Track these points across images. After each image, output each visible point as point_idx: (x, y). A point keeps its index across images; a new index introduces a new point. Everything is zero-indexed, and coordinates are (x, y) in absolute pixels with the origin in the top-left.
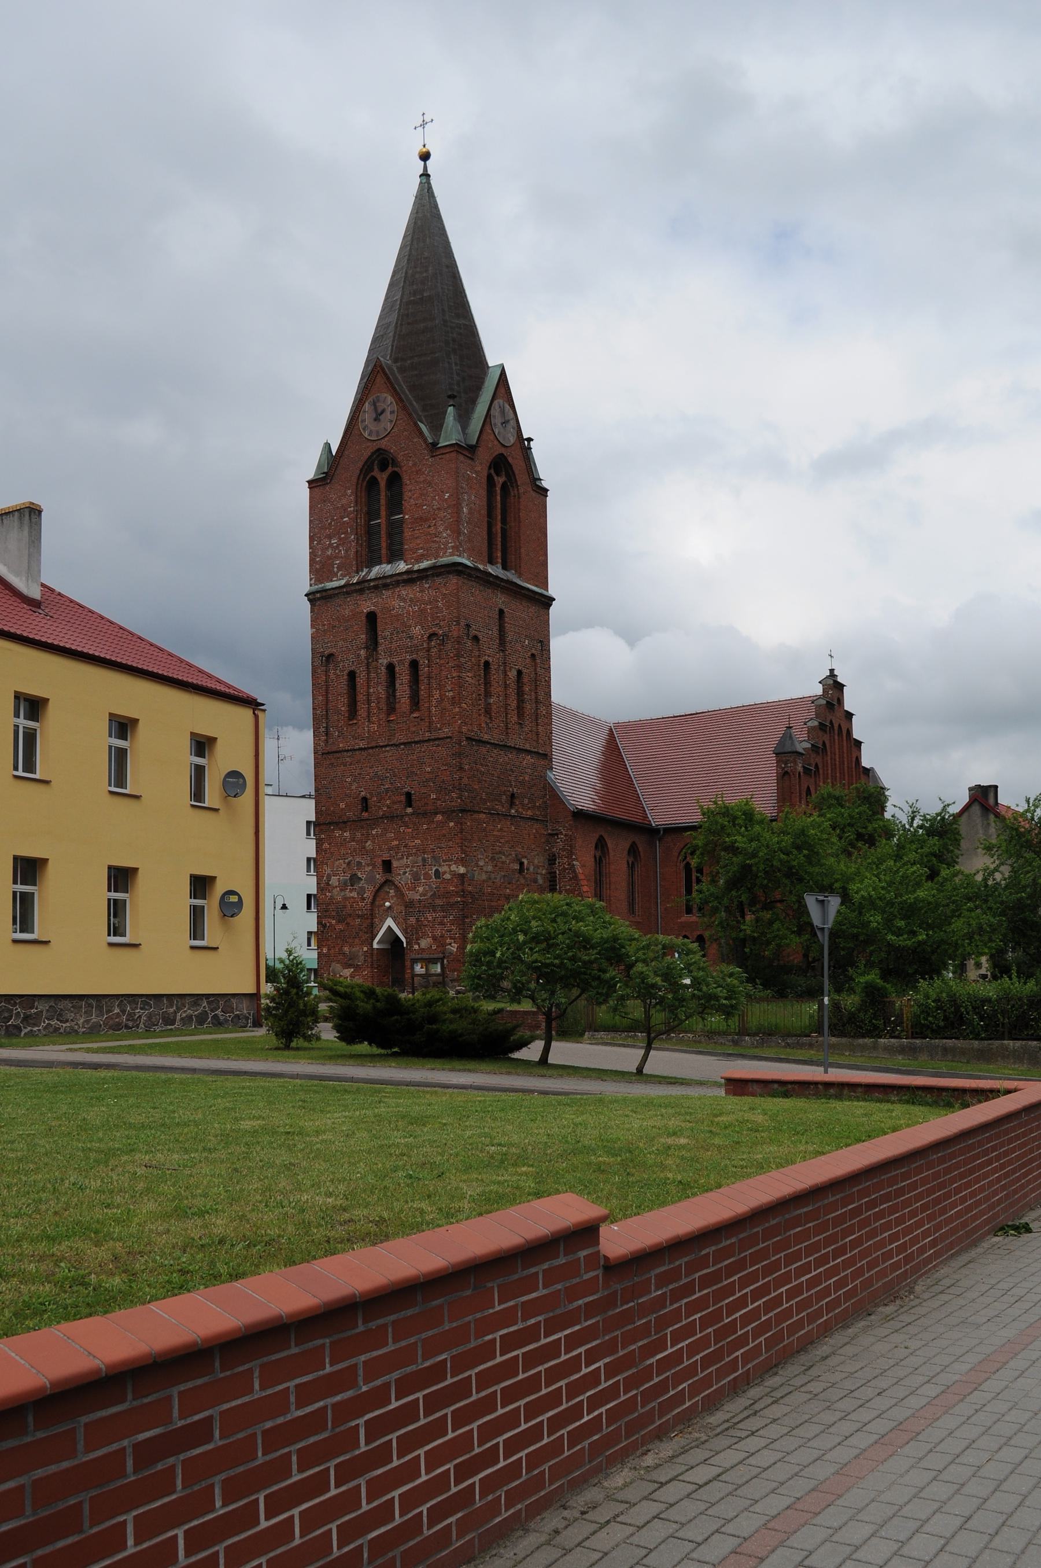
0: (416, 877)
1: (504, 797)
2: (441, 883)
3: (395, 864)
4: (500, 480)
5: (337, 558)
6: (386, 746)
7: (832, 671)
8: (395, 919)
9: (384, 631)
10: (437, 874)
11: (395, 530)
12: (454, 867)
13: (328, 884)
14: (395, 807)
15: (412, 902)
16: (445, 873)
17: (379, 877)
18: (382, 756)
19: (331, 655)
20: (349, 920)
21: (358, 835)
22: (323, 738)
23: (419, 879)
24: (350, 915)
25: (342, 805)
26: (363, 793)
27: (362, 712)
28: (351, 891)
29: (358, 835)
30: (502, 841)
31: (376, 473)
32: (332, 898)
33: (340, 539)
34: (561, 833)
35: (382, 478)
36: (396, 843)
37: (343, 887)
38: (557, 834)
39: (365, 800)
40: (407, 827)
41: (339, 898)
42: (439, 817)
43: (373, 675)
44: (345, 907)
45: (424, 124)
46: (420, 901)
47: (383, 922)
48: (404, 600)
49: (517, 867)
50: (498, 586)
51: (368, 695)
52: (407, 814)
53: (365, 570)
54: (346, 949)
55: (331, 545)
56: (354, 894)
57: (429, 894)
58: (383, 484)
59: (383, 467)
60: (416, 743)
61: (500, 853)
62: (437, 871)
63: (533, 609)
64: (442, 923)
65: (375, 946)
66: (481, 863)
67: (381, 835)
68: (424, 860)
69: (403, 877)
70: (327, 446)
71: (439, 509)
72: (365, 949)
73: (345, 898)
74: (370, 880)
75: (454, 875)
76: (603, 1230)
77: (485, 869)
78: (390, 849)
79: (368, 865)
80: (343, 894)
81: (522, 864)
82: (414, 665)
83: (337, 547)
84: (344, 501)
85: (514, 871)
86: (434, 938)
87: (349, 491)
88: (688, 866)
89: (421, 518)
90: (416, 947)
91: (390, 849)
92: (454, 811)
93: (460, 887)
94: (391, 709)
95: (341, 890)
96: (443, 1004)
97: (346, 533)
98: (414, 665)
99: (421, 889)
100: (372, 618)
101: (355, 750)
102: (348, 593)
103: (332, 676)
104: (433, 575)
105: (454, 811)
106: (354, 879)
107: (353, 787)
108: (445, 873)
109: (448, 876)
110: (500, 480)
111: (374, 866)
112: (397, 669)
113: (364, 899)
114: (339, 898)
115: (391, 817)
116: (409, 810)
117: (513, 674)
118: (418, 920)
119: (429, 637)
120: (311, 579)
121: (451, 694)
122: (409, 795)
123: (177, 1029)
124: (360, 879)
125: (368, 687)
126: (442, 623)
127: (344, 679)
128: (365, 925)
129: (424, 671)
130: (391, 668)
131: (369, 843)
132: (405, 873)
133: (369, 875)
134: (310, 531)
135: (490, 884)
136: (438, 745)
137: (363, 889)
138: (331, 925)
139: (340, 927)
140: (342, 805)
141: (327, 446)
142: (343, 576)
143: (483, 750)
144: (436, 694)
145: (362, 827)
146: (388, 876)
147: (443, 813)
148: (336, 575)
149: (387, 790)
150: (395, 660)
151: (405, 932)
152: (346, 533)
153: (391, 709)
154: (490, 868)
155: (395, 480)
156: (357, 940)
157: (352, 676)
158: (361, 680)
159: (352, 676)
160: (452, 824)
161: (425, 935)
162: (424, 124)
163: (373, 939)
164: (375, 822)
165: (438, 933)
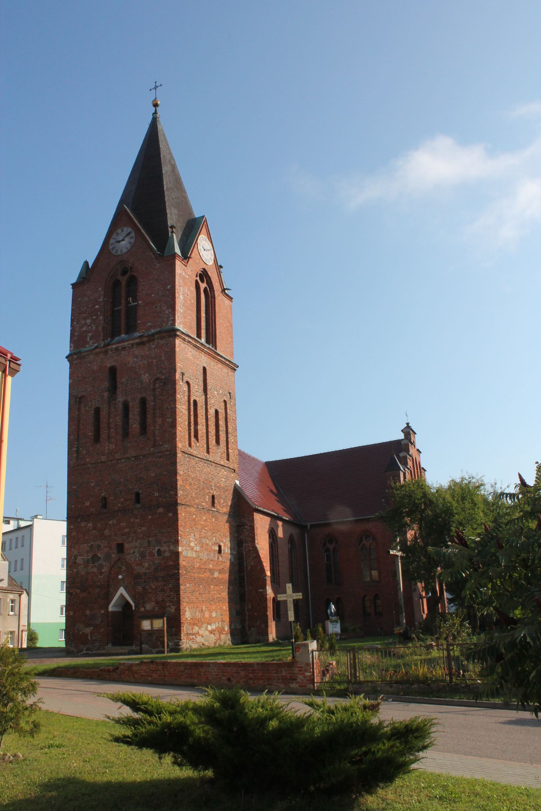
0: (143, 555)
1: (207, 497)
3: (126, 546)
4: (203, 286)
5: (89, 332)
7: (408, 424)
8: (126, 588)
9: (122, 380)
11: (131, 312)
13: (75, 563)
14: (128, 503)
16: (164, 552)
19: (82, 397)
23: (146, 557)
25: (87, 504)
26: (103, 494)
27: (104, 435)
28: (92, 567)
29: (99, 525)
30: (206, 528)
33: (93, 320)
34: (247, 525)
36: (127, 530)
38: (243, 526)
39: (104, 499)
41: (83, 573)
42: (161, 510)
43: (112, 410)
45: (156, 88)
46: (145, 574)
47: (116, 590)
48: (137, 357)
49: (217, 548)
50: (203, 350)
51: (109, 424)
53: (109, 339)
55: (86, 323)
56: (95, 570)
58: (124, 284)
59: (124, 273)
61: (205, 537)
62: (159, 550)
63: (226, 370)
64: (163, 590)
65: (111, 608)
66: (192, 544)
68: (149, 542)
70: (86, 263)
71: (163, 296)
72: (103, 612)
74: (108, 557)
77: (195, 549)
79: (106, 547)
81: (220, 547)
82: (143, 402)
83: (90, 325)
85: (215, 551)
86: (157, 602)
88: (327, 550)
90: (142, 609)
91: (123, 535)
94: (126, 434)
96: (441, 620)
97: (97, 315)
98: (143, 402)
99: (146, 565)
100: (113, 371)
101: (98, 463)
106: (95, 559)
107: (96, 490)
108: (164, 552)
109: (167, 554)
110: (203, 286)
112: (131, 404)
113: (101, 573)
114: (83, 573)
116: (138, 506)
117: (212, 412)
118: (144, 588)
119: (154, 381)
120: (70, 347)
122: (138, 495)
124: (100, 558)
125: (109, 418)
126: (164, 371)
129: (150, 404)
130: (126, 407)
131: (107, 530)
132: (134, 553)
134: (72, 306)
135: (199, 560)
140: (87, 504)
141: (86, 263)
142: (93, 343)
143: (193, 462)
144: (159, 421)
148: (88, 343)
152: (97, 315)
153: (126, 434)
154: (198, 548)
157: (97, 411)
158: (104, 413)
159: (97, 411)
162: (156, 88)
163: (109, 604)
165: (160, 599)
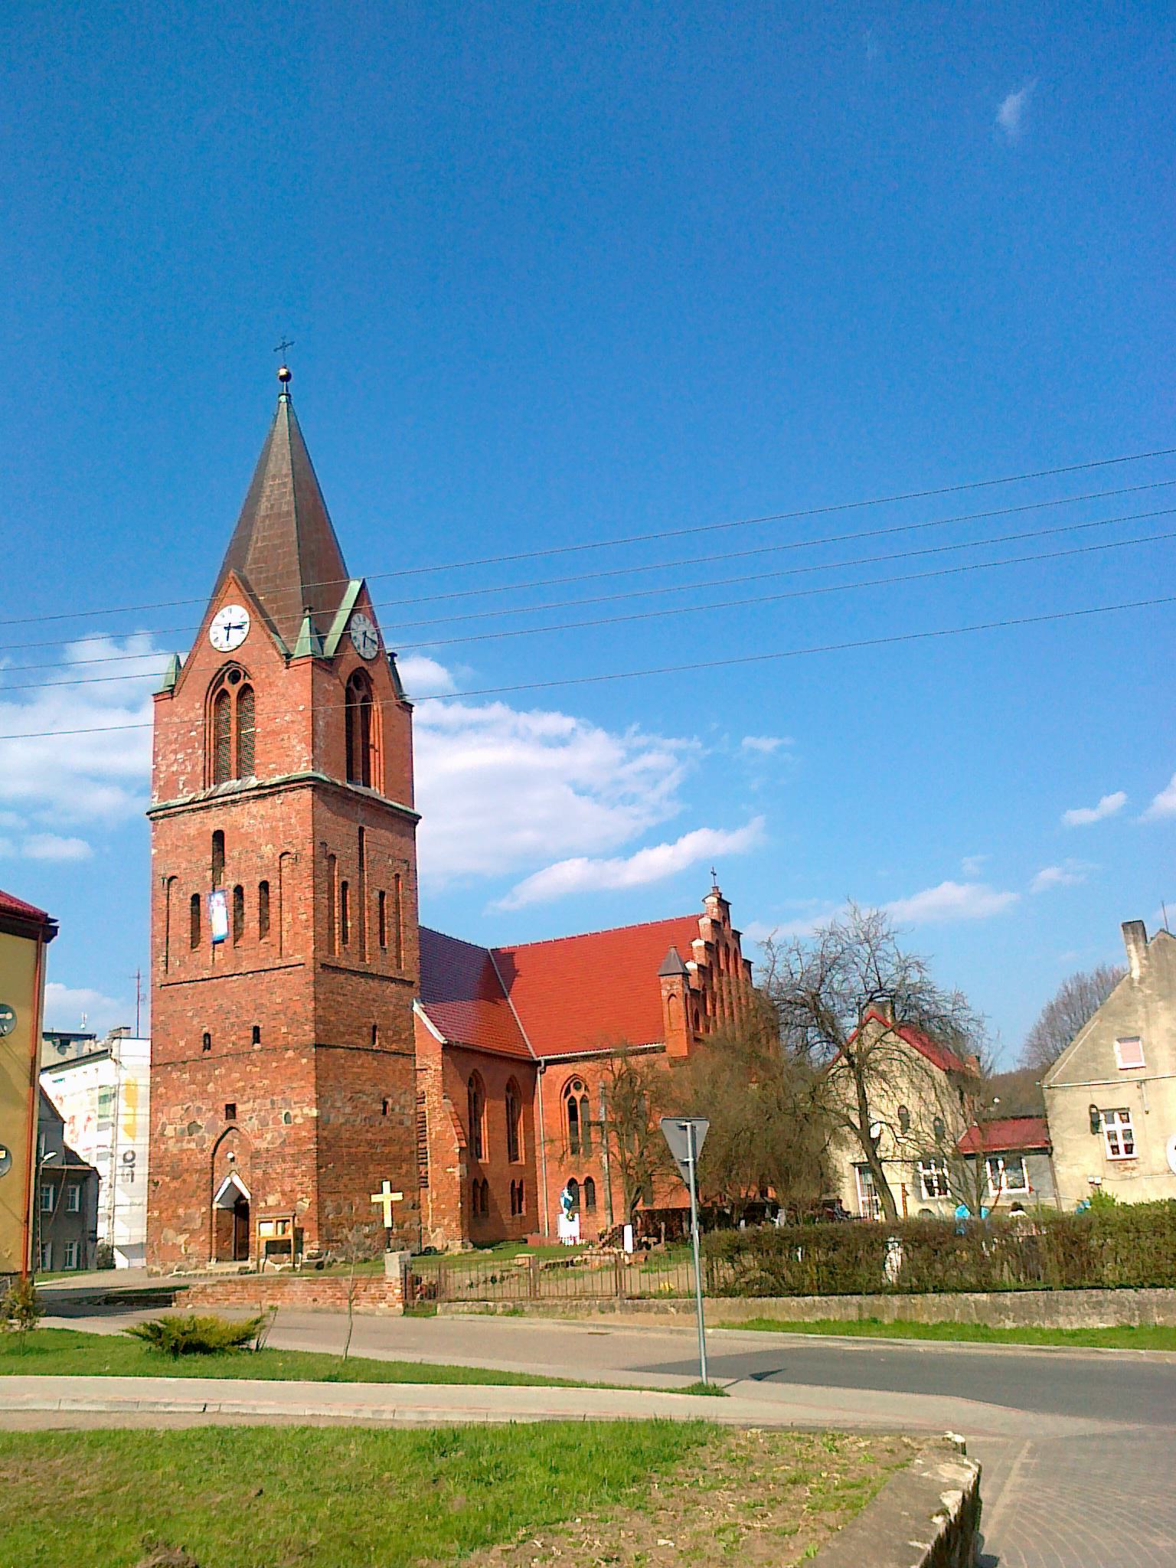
0: (264, 1123)
3: (240, 1108)
5: (183, 773)
12: (306, 1110)
13: (162, 1135)
14: (242, 1042)
17: (222, 1124)
21: (199, 1076)
25: (182, 1043)
28: (189, 1142)
31: (227, 685)
39: (207, 1035)
42: (290, 1054)
44: (181, 1160)
48: (254, 817)
54: (181, 1211)
56: (193, 1145)
57: (279, 1141)
64: (292, 1175)
68: (273, 1102)
72: (203, 1210)
73: (182, 1151)
75: (305, 1117)
82: (264, 886)
84: (192, 715)
86: (283, 1193)
89: (273, 732)
92: (306, 1046)
98: (264, 886)
99: (269, 1137)
100: (219, 836)
102: (193, 810)
104: (286, 790)
105: (306, 1046)
106: (193, 1128)
111: (216, 1112)
113: (203, 1150)
129: (274, 892)
133: (211, 1122)
137: (203, 1138)
146: (232, 1122)
150: (243, 883)
151: (250, 1187)
160: (304, 1061)
161: (273, 1192)
164: (221, 1059)
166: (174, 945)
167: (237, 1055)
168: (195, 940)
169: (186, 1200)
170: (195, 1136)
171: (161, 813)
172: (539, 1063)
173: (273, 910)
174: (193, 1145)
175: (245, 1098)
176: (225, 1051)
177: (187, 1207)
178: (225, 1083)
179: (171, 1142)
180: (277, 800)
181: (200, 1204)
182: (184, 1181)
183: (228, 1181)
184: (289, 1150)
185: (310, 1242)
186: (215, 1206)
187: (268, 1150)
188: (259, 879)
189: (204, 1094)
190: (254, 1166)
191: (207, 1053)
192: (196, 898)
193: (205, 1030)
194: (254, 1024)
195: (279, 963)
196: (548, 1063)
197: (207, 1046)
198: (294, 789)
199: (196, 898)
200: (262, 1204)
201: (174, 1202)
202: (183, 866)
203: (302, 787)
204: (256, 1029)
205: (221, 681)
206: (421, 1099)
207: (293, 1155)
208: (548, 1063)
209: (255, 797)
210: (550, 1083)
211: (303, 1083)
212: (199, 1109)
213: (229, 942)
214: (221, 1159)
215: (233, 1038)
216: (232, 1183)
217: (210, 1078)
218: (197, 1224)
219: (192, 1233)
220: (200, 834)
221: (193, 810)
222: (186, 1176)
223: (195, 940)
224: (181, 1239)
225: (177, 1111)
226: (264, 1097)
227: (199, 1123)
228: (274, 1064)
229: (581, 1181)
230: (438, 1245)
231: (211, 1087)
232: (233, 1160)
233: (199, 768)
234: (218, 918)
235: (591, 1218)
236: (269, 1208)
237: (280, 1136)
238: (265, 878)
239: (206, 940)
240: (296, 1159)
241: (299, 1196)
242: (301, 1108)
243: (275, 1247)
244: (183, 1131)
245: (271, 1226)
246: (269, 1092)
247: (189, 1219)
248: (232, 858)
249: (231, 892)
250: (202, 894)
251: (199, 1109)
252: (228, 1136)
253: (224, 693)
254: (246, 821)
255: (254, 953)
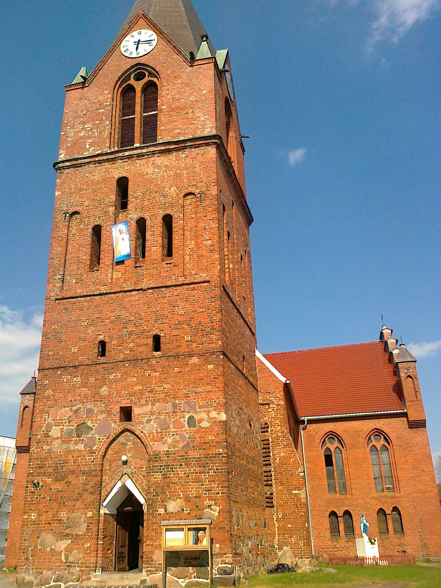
0: (164, 427)
2: (198, 432)
3: (136, 411)
5: (89, 137)
6: (131, 291)
10: (191, 421)
12: (213, 414)
13: (47, 435)
14: (140, 349)
15: (156, 457)
16: (201, 421)
17: (116, 425)
18: (127, 300)
20: (70, 478)
21: (92, 380)
22: (58, 285)
24: (72, 472)
25: (74, 350)
28: (76, 443)
29: (92, 380)
31: (132, 81)
32: (50, 451)
35: (138, 86)
37: (66, 439)
39: (103, 344)
40: (155, 371)
42: (195, 360)
44: (66, 462)
48: (159, 167)
52: (154, 357)
54: (63, 515)
56: (81, 447)
57: (181, 445)
60: (166, 287)
62: (191, 418)
64: (198, 480)
67: (121, 380)
68: (175, 406)
69: (145, 423)
72: (90, 514)
73: (68, 452)
74: (103, 428)
75: (214, 422)
76: (125, 261)
78: (133, 394)
79: (102, 412)
80: (65, 446)
82: (168, 220)
83: (91, 130)
84: (101, 98)
86: (187, 499)
87: (106, 92)
89: (178, 108)
91: (133, 394)
92: (213, 353)
93: (223, 437)
95: (63, 442)
98: (168, 220)
99: (170, 440)
100: (123, 185)
102: (99, 162)
103: (74, 231)
104: (191, 147)
105: (213, 353)
106: (82, 429)
107: (90, 331)
109: (205, 424)
111: (109, 413)
113: (92, 452)
115: (134, 361)
118: (165, 477)
121: (209, 242)
123: (150, 74)
124: (90, 429)
126: (199, 185)
127: (88, 238)
128: (92, 484)
129: (176, 225)
131: (105, 388)
132: (148, 421)
133: (104, 423)
136: (194, 289)
137: (92, 440)
138: (45, 485)
139: (59, 486)
145: (97, 372)
146: (127, 425)
147: (200, 356)
149: (131, 333)
150: (146, 216)
151: (146, 493)
155: (151, 89)
156: (79, 504)
160: (211, 367)
161: (174, 497)
164: (116, 364)
165: (192, 494)
166: (72, 267)
167: (134, 361)
168: (96, 258)
169: (71, 503)
170: (84, 437)
171: (68, 164)
172: (303, 422)
173: (176, 237)
174: (81, 447)
175: (143, 401)
176: (122, 357)
177: (71, 510)
178: (119, 386)
179: (56, 444)
180: (182, 155)
181: (86, 507)
182: (68, 483)
183: (119, 484)
184: (194, 454)
185: (221, 555)
186: (102, 512)
187: (168, 454)
188: (162, 213)
189: (96, 397)
190: (150, 471)
191: (102, 359)
192: (97, 230)
193: (101, 338)
194: (154, 333)
195: (181, 280)
196: (310, 422)
197: (103, 353)
198: (199, 146)
199: (97, 230)
200: (162, 511)
201: (55, 505)
202: (86, 203)
203: (207, 145)
204: (157, 339)
205: (128, 78)
206: (265, 428)
207: (198, 459)
208: (310, 422)
209: (161, 152)
210: (310, 438)
211: (209, 388)
212: (90, 411)
213: (129, 263)
214: (111, 462)
215: (131, 345)
216: (124, 487)
217: (103, 382)
218: (82, 529)
219: (76, 538)
220: (105, 180)
221: (99, 162)
222: (70, 478)
223: (96, 258)
224: (63, 545)
225: (66, 412)
226: (165, 401)
227: (89, 424)
228: (177, 370)
229: (340, 513)
230: (288, 561)
231: (104, 390)
232: (125, 463)
233: (106, 134)
234: (121, 240)
235: (350, 544)
236: (170, 516)
237: (183, 438)
238: (168, 212)
239: (106, 259)
240: (203, 464)
241: (207, 502)
242: (209, 412)
243: (175, 559)
244: (70, 433)
245: (180, 535)
246: (167, 396)
247: (72, 524)
248: (136, 198)
249: (133, 223)
250: (104, 225)
251: (90, 411)
252: (121, 439)
253: (131, 89)
254: (149, 171)
255: (155, 269)
